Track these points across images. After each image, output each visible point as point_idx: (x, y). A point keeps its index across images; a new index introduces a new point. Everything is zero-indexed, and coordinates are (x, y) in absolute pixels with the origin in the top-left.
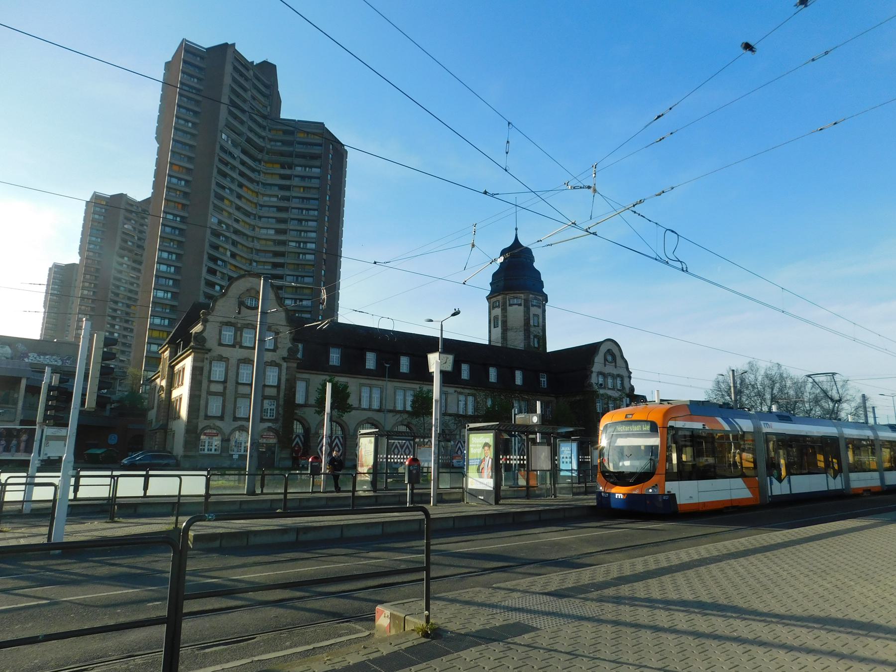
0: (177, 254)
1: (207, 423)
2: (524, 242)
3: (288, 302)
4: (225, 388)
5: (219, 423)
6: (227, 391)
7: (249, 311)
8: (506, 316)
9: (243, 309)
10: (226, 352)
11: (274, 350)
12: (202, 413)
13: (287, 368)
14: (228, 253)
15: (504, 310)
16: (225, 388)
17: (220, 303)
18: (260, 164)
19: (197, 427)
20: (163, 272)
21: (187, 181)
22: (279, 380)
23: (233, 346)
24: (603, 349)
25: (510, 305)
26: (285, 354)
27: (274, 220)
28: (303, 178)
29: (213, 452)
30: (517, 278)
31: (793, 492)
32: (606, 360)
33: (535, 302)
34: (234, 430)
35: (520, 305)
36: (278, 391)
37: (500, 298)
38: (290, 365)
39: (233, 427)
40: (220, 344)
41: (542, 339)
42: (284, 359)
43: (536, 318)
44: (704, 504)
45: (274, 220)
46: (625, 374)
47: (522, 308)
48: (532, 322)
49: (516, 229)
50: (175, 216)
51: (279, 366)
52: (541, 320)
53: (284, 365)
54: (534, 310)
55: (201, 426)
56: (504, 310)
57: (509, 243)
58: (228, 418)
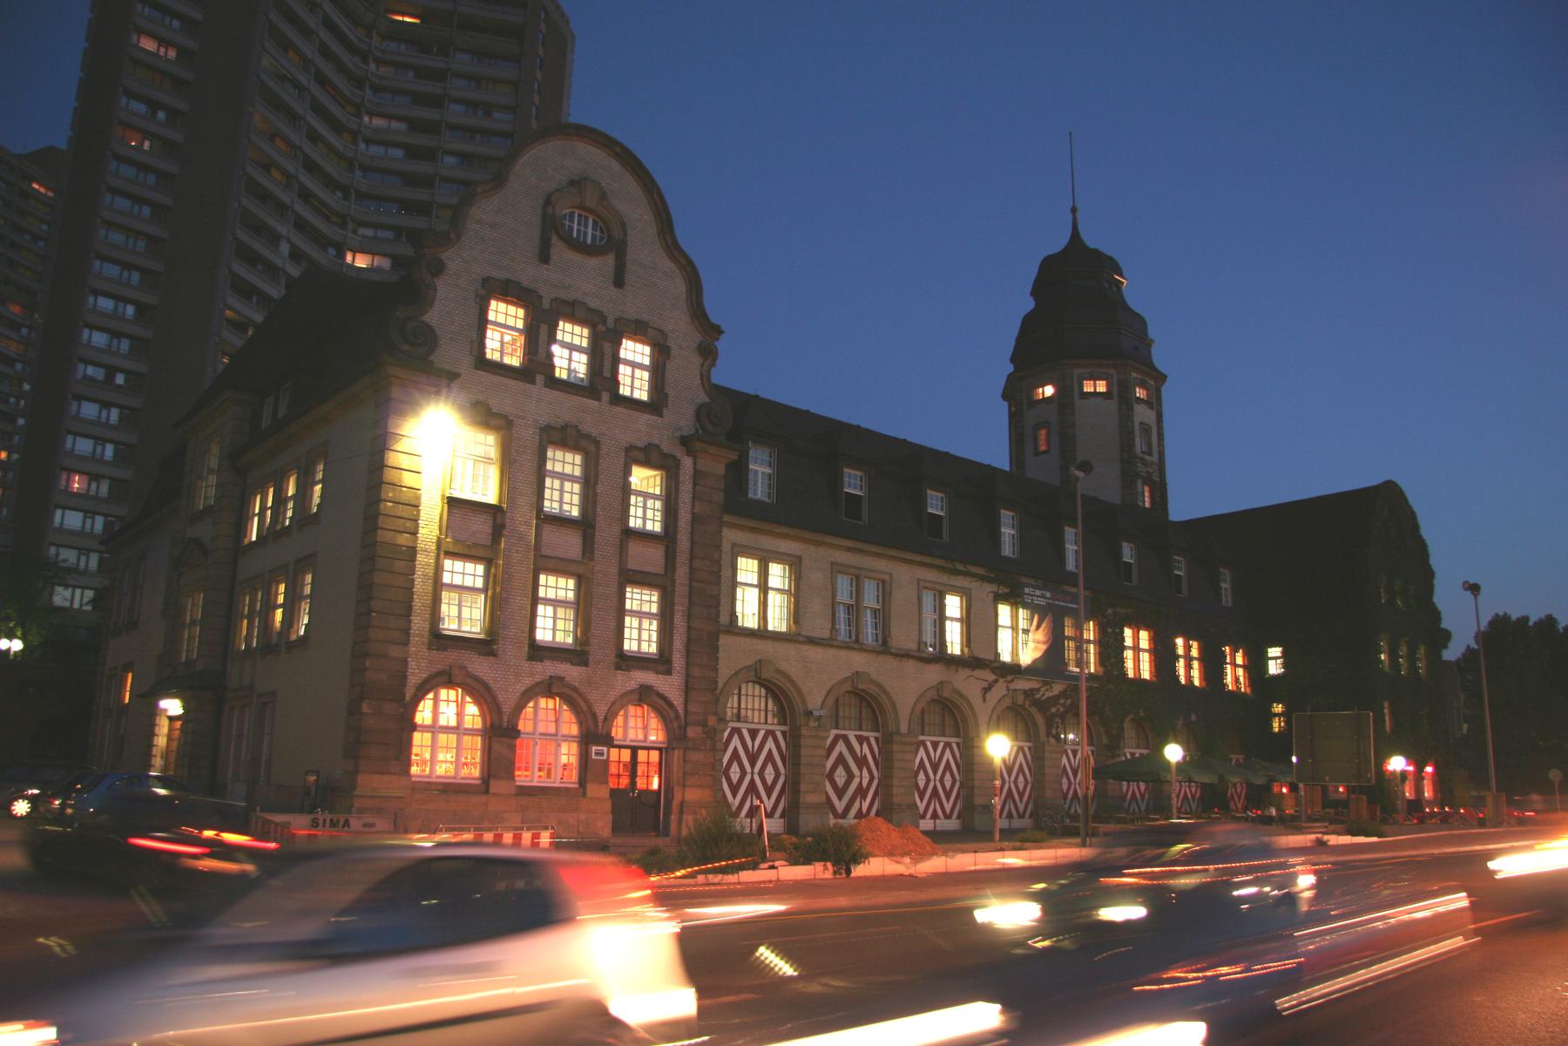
0: (144, 271)
2: (1091, 240)
3: (282, 412)
7: (578, 258)
9: (558, 249)
13: (697, 475)
14: (285, 248)
18: (365, 61)
21: (172, 113)
26: (687, 424)
28: (473, 105)
30: (1078, 313)
31: (739, 591)
34: (530, 694)
39: (527, 682)
42: (685, 442)
49: (1074, 210)
50: (154, 106)
53: (687, 463)
57: (1058, 243)
58: (513, 652)
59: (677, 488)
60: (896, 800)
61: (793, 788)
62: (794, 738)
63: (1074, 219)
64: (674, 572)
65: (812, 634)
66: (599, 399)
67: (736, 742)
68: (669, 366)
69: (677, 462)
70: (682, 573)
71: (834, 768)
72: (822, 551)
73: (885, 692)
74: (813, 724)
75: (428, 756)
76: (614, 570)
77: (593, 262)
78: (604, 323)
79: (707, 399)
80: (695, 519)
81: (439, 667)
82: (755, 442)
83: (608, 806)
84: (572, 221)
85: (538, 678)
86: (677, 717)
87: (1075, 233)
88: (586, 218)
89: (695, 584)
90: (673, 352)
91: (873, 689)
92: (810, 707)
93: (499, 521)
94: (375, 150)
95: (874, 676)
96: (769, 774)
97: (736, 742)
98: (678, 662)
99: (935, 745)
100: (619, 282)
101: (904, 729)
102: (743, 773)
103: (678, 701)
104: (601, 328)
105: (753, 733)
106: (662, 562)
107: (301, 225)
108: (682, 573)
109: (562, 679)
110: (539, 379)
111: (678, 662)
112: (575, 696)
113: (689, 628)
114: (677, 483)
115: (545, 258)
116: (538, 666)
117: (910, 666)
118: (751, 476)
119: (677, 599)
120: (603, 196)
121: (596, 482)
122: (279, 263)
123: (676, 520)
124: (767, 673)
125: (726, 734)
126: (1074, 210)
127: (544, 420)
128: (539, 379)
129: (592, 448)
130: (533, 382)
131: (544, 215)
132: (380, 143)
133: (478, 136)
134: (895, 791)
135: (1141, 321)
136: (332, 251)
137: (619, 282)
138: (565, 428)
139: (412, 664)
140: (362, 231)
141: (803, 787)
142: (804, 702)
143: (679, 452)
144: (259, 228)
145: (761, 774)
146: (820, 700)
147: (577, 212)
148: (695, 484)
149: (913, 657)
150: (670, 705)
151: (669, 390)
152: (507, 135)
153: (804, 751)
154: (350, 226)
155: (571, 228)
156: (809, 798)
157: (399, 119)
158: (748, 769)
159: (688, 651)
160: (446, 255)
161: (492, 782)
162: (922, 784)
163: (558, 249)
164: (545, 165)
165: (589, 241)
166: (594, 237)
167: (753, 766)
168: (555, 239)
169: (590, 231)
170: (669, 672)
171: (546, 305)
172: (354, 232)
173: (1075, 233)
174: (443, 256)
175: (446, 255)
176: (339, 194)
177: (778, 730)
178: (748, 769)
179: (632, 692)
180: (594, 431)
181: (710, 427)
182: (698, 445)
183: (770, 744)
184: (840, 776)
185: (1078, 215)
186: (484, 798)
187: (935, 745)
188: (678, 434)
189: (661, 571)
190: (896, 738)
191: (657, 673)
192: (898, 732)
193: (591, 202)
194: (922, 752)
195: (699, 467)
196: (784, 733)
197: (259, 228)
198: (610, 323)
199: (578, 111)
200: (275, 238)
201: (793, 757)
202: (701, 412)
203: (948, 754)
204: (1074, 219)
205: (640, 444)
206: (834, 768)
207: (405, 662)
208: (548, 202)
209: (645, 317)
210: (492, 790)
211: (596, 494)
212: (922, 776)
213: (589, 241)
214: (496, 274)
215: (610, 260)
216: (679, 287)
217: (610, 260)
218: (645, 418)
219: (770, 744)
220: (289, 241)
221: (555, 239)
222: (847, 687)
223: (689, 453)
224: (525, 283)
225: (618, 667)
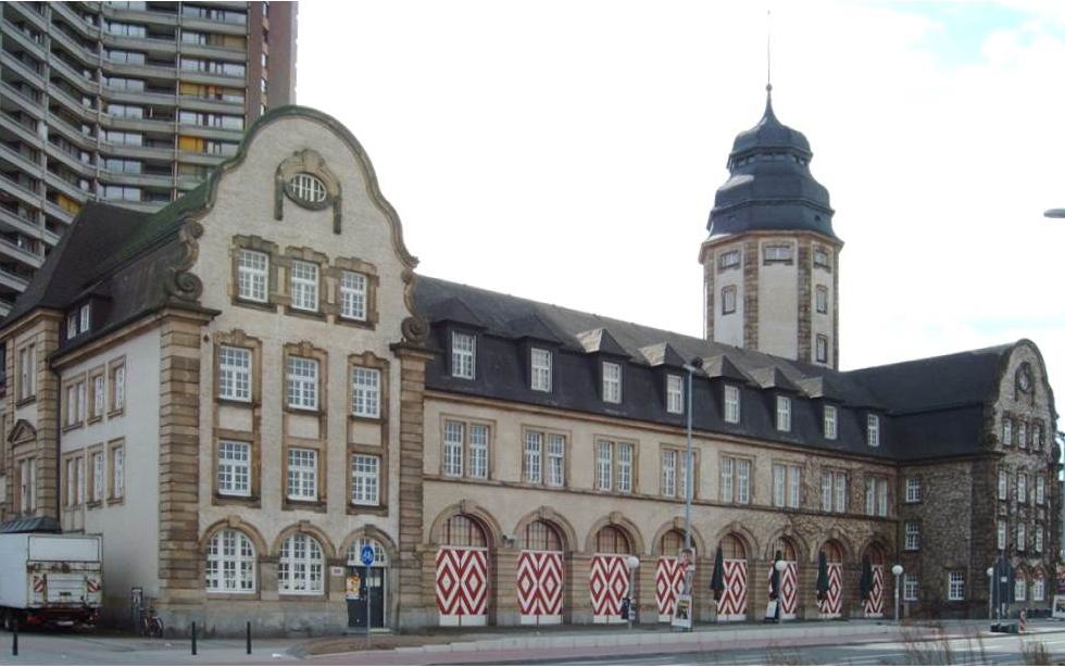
1: (221, 512)
2: (785, 118)
4: (257, 422)
5: (247, 514)
6: (264, 429)
8: (756, 288)
9: (290, 209)
10: (253, 323)
11: (369, 325)
12: (205, 488)
13: (404, 372)
14: (43, 131)
15: (751, 272)
16: (257, 422)
17: (229, 184)
19: (196, 524)
20: (133, 39)
22: (385, 402)
23: (270, 307)
24: (1014, 363)
25: (767, 262)
27: (140, 85)
29: (239, 590)
32: (1018, 386)
33: (819, 258)
35: (789, 262)
36: (385, 436)
37: (741, 245)
38: (408, 364)
40: (237, 301)
41: (831, 343)
42: (394, 348)
43: (822, 295)
44: (570, 635)
45: (140, 85)
46: (1046, 416)
47: (793, 270)
48: (814, 302)
49: (769, 88)
51: (381, 365)
52: (830, 299)
53: (396, 365)
54: (819, 276)
55: (205, 521)
56: (751, 272)
57: (751, 121)
59: (388, 384)
60: (575, 601)
61: (492, 592)
62: (493, 556)
63: (769, 95)
64: (388, 443)
65: (505, 479)
66: (326, 321)
67: (446, 559)
68: (379, 291)
69: (387, 363)
70: (394, 445)
71: (522, 578)
72: (513, 415)
73: (565, 521)
74: (507, 546)
75: (979, 495)
76: (344, 445)
77: (314, 215)
78: (327, 262)
79: (409, 315)
80: (404, 404)
81: (221, 518)
82: (458, 332)
83: (346, 607)
84: (298, 183)
85: (292, 522)
86: (394, 546)
87: (769, 113)
88: (309, 180)
89: (404, 452)
90: (381, 280)
91: (556, 519)
92: (505, 533)
93: (256, 414)
94: (116, 29)
95: (556, 509)
96: (474, 583)
97: (446, 559)
98: (393, 507)
99: (608, 560)
100: (337, 231)
101: (581, 548)
102: (532, 584)
103: (394, 534)
104: (325, 266)
105: (460, 554)
106: (379, 437)
107: (56, 108)
108: (394, 445)
109: (308, 522)
110: (280, 309)
111: (393, 507)
112: (319, 534)
113: (401, 483)
114: (388, 379)
115: (279, 217)
116: (290, 514)
117: (586, 501)
118: (455, 360)
119: (391, 463)
120: (322, 163)
121: (327, 382)
122: (39, 145)
123: (388, 406)
124: (470, 510)
125: (438, 555)
126: (769, 88)
127: (285, 340)
128: (280, 309)
129: (322, 357)
130: (275, 311)
131: (277, 183)
132: (122, 23)
133: (214, 13)
134: (574, 594)
135: (824, 193)
136: (86, 129)
137: (337, 231)
138: (300, 345)
139: (202, 515)
140: (112, 108)
141: (499, 592)
142: (499, 529)
143: (389, 356)
144: (18, 115)
145: (532, 584)
146: (513, 527)
147: (302, 176)
148: (402, 379)
149: (589, 494)
150: (389, 538)
151: (380, 309)
152: (243, 38)
153: (499, 566)
154: (100, 104)
155: (298, 190)
156: (503, 600)
157: (138, 24)
158: (541, 588)
159: (400, 500)
160: (204, 221)
161: (262, 592)
162: (597, 589)
163: (290, 209)
164: (275, 142)
165: (312, 199)
166: (316, 194)
167: (538, 578)
168: (285, 200)
169: (312, 190)
170: (386, 515)
171: (282, 252)
172: (105, 110)
173: (769, 113)
174: (201, 222)
175: (204, 221)
176: (86, 73)
177: (480, 550)
178: (541, 588)
179: (359, 530)
180: (324, 346)
181: (412, 336)
182: (403, 352)
183: (474, 560)
184: (446, 582)
185: (772, 92)
186: (258, 603)
187: (608, 560)
188: (388, 342)
189: (378, 443)
190: (574, 556)
191: (378, 515)
192: (577, 551)
193: (312, 168)
194: (661, 568)
195: (405, 367)
196: (485, 553)
197: (18, 115)
198: (332, 262)
199: (303, 96)
200: (33, 122)
201: (493, 572)
202: (407, 326)
203: (737, 570)
204: (769, 95)
205: (359, 352)
206: (522, 578)
207: (197, 514)
208: (279, 171)
209: (358, 255)
210: (263, 597)
211: (326, 391)
212: (597, 582)
213: (312, 199)
214: (242, 232)
215: (330, 213)
216: (386, 228)
217: (330, 213)
218: (361, 333)
219: (474, 560)
220: (46, 123)
221: (285, 200)
222: (535, 517)
223: (397, 356)
224: (264, 238)
225: (348, 513)
